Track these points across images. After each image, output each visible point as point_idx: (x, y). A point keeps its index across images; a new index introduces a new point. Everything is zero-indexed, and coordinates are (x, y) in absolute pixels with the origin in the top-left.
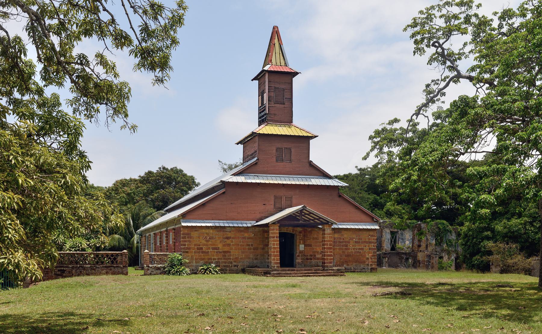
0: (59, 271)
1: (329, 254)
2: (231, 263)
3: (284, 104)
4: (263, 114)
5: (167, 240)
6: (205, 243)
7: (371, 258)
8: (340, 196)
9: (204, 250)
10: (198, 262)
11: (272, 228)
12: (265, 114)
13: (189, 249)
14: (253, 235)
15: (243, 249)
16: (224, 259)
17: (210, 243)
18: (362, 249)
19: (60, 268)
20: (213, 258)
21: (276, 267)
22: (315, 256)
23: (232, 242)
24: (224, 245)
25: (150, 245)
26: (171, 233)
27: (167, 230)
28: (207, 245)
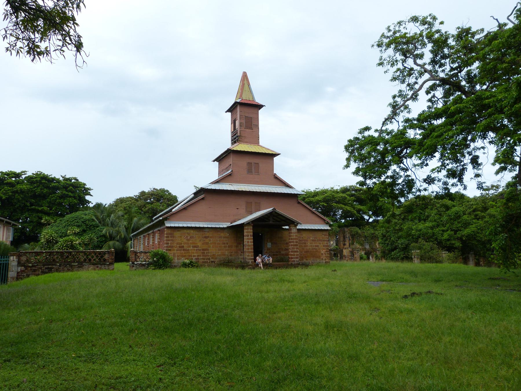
0: (46, 268)
1: (295, 250)
2: (209, 259)
3: (252, 129)
4: (235, 137)
5: (153, 240)
6: (186, 241)
7: (325, 254)
8: (299, 203)
9: (185, 248)
10: (180, 259)
11: (246, 227)
12: (237, 137)
13: (172, 247)
14: (228, 234)
15: (220, 247)
16: (203, 256)
17: (191, 242)
18: (318, 246)
19: (48, 266)
20: (193, 255)
21: (250, 263)
22: (280, 252)
23: (210, 240)
24: (203, 244)
25: (140, 245)
26: (156, 234)
27: (153, 232)
28: (188, 244)
